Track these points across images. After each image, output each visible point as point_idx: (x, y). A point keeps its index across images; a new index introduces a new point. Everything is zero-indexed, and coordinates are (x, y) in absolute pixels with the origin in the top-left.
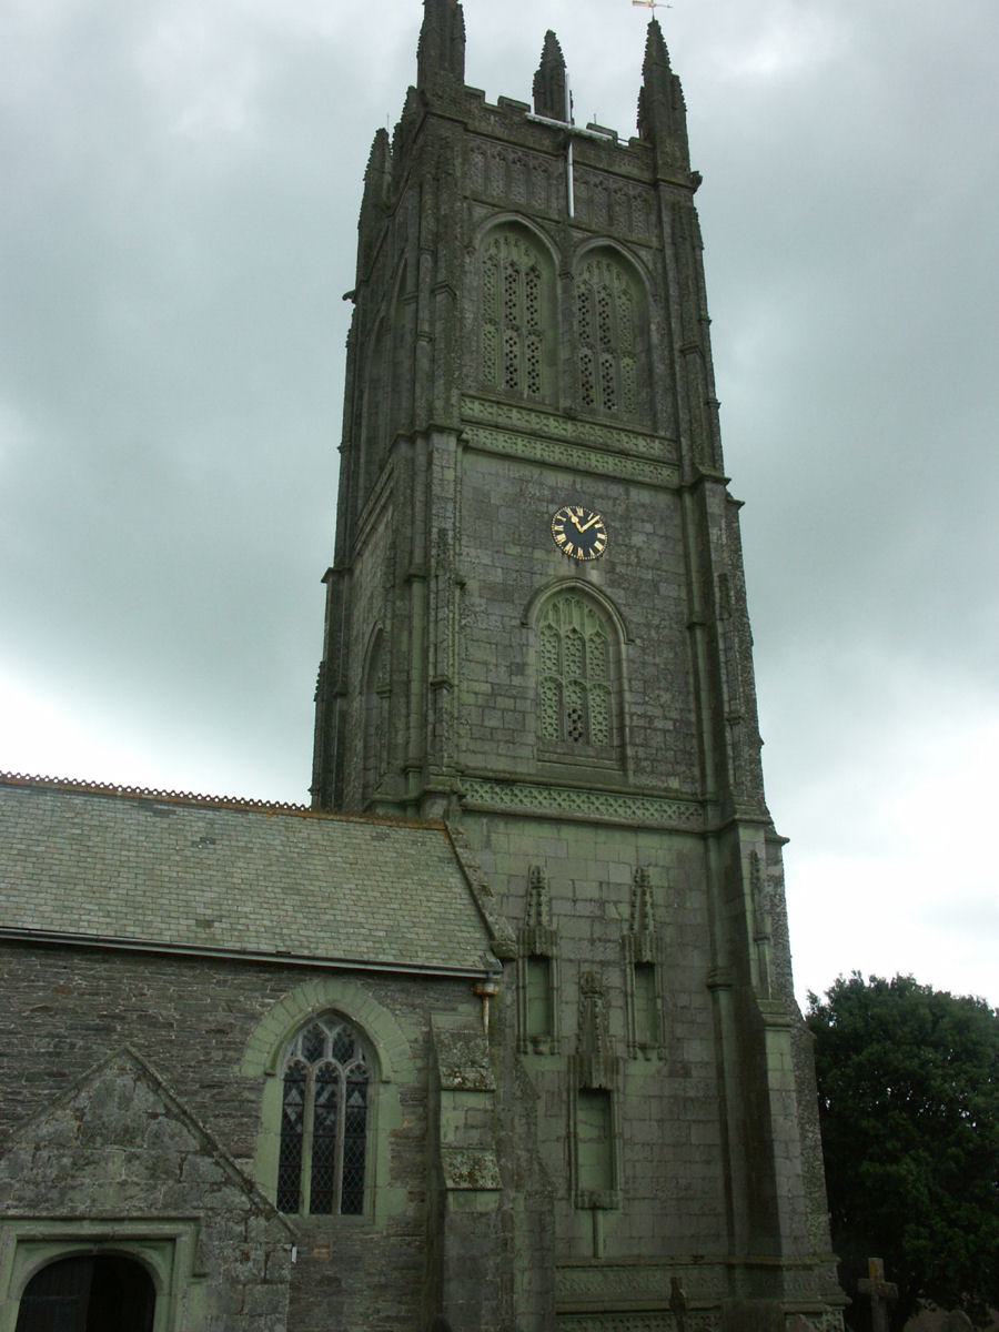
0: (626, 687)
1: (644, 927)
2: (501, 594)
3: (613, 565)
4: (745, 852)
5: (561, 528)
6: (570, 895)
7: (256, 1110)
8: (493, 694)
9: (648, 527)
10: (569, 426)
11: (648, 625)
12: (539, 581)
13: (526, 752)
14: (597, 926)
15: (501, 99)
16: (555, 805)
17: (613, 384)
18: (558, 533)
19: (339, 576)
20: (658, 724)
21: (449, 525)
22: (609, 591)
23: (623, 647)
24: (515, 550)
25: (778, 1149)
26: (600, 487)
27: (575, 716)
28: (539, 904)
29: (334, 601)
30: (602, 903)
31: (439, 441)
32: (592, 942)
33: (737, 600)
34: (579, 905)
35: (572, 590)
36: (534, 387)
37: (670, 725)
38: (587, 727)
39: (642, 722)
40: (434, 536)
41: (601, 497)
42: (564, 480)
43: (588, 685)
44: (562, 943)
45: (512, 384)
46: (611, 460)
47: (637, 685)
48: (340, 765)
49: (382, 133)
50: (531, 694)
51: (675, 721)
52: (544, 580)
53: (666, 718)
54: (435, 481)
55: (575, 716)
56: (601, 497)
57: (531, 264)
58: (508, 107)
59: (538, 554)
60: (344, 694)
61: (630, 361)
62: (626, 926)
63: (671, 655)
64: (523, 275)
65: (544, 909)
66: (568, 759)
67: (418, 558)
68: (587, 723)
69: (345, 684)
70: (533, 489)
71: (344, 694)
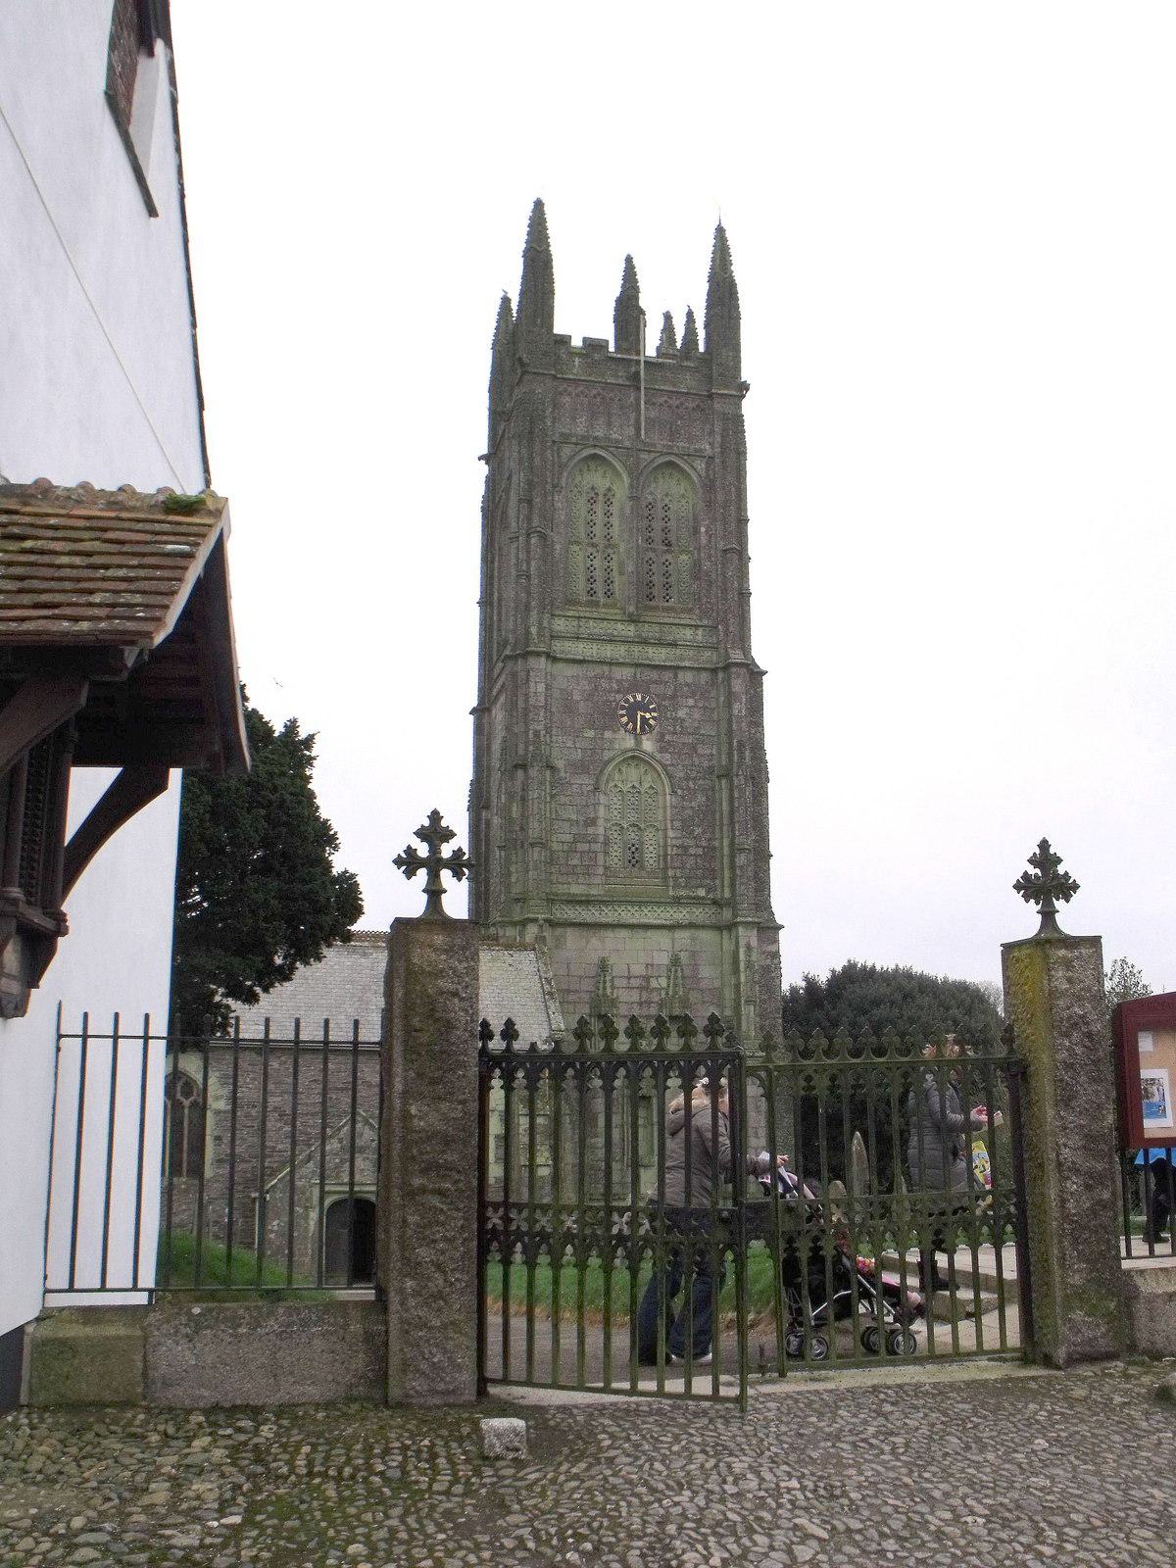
0: (669, 826)
1: (675, 993)
2: (580, 768)
3: (663, 736)
4: (742, 942)
5: (624, 712)
6: (626, 974)
7: (194, 681)
8: (575, 842)
9: (691, 702)
10: (632, 628)
11: (687, 779)
12: (607, 755)
13: (598, 880)
14: (644, 993)
15: (585, 340)
16: (616, 914)
17: (672, 580)
18: (622, 716)
19: (480, 712)
20: (692, 851)
21: (541, 727)
22: (658, 756)
23: (668, 797)
24: (591, 734)
25: (750, 1132)
26: (654, 675)
27: (633, 849)
28: (605, 982)
29: (479, 730)
30: (647, 978)
31: (532, 662)
32: (641, 1004)
33: (753, 758)
34: (632, 981)
35: (633, 757)
36: (609, 594)
37: (700, 851)
38: (641, 856)
39: (680, 851)
40: (531, 735)
41: (655, 682)
42: (625, 673)
43: (642, 826)
44: (620, 1005)
45: (591, 592)
46: (664, 651)
47: (677, 824)
48: (487, 860)
49: (506, 301)
50: (601, 839)
51: (704, 848)
52: (611, 754)
53: (697, 846)
54: (532, 694)
55: (633, 849)
56: (655, 682)
57: (608, 485)
58: (593, 346)
59: (608, 734)
60: (487, 807)
61: (686, 558)
62: (663, 993)
63: (704, 799)
64: (601, 497)
65: (608, 984)
66: (628, 881)
67: (521, 752)
68: (642, 853)
69: (488, 799)
70: (604, 684)
71: (487, 807)
